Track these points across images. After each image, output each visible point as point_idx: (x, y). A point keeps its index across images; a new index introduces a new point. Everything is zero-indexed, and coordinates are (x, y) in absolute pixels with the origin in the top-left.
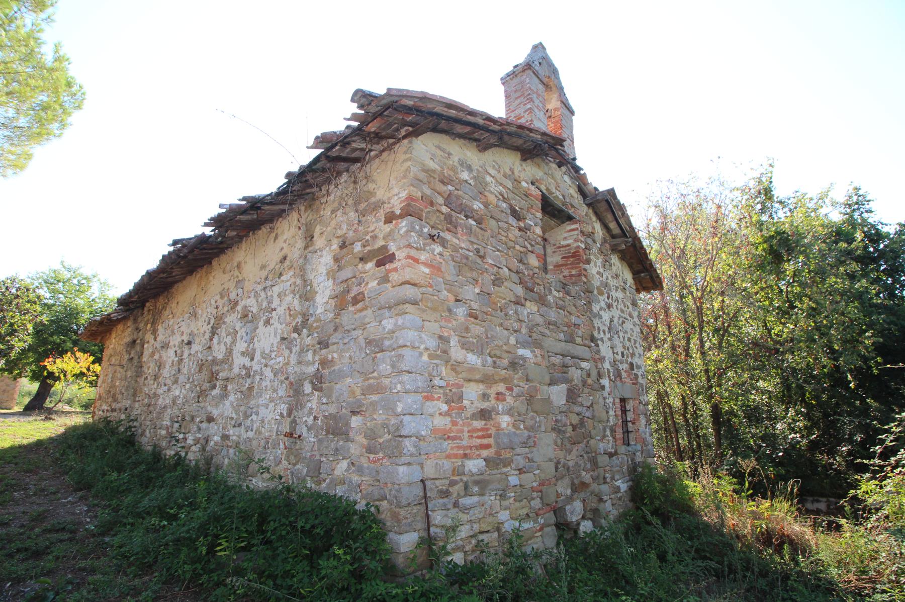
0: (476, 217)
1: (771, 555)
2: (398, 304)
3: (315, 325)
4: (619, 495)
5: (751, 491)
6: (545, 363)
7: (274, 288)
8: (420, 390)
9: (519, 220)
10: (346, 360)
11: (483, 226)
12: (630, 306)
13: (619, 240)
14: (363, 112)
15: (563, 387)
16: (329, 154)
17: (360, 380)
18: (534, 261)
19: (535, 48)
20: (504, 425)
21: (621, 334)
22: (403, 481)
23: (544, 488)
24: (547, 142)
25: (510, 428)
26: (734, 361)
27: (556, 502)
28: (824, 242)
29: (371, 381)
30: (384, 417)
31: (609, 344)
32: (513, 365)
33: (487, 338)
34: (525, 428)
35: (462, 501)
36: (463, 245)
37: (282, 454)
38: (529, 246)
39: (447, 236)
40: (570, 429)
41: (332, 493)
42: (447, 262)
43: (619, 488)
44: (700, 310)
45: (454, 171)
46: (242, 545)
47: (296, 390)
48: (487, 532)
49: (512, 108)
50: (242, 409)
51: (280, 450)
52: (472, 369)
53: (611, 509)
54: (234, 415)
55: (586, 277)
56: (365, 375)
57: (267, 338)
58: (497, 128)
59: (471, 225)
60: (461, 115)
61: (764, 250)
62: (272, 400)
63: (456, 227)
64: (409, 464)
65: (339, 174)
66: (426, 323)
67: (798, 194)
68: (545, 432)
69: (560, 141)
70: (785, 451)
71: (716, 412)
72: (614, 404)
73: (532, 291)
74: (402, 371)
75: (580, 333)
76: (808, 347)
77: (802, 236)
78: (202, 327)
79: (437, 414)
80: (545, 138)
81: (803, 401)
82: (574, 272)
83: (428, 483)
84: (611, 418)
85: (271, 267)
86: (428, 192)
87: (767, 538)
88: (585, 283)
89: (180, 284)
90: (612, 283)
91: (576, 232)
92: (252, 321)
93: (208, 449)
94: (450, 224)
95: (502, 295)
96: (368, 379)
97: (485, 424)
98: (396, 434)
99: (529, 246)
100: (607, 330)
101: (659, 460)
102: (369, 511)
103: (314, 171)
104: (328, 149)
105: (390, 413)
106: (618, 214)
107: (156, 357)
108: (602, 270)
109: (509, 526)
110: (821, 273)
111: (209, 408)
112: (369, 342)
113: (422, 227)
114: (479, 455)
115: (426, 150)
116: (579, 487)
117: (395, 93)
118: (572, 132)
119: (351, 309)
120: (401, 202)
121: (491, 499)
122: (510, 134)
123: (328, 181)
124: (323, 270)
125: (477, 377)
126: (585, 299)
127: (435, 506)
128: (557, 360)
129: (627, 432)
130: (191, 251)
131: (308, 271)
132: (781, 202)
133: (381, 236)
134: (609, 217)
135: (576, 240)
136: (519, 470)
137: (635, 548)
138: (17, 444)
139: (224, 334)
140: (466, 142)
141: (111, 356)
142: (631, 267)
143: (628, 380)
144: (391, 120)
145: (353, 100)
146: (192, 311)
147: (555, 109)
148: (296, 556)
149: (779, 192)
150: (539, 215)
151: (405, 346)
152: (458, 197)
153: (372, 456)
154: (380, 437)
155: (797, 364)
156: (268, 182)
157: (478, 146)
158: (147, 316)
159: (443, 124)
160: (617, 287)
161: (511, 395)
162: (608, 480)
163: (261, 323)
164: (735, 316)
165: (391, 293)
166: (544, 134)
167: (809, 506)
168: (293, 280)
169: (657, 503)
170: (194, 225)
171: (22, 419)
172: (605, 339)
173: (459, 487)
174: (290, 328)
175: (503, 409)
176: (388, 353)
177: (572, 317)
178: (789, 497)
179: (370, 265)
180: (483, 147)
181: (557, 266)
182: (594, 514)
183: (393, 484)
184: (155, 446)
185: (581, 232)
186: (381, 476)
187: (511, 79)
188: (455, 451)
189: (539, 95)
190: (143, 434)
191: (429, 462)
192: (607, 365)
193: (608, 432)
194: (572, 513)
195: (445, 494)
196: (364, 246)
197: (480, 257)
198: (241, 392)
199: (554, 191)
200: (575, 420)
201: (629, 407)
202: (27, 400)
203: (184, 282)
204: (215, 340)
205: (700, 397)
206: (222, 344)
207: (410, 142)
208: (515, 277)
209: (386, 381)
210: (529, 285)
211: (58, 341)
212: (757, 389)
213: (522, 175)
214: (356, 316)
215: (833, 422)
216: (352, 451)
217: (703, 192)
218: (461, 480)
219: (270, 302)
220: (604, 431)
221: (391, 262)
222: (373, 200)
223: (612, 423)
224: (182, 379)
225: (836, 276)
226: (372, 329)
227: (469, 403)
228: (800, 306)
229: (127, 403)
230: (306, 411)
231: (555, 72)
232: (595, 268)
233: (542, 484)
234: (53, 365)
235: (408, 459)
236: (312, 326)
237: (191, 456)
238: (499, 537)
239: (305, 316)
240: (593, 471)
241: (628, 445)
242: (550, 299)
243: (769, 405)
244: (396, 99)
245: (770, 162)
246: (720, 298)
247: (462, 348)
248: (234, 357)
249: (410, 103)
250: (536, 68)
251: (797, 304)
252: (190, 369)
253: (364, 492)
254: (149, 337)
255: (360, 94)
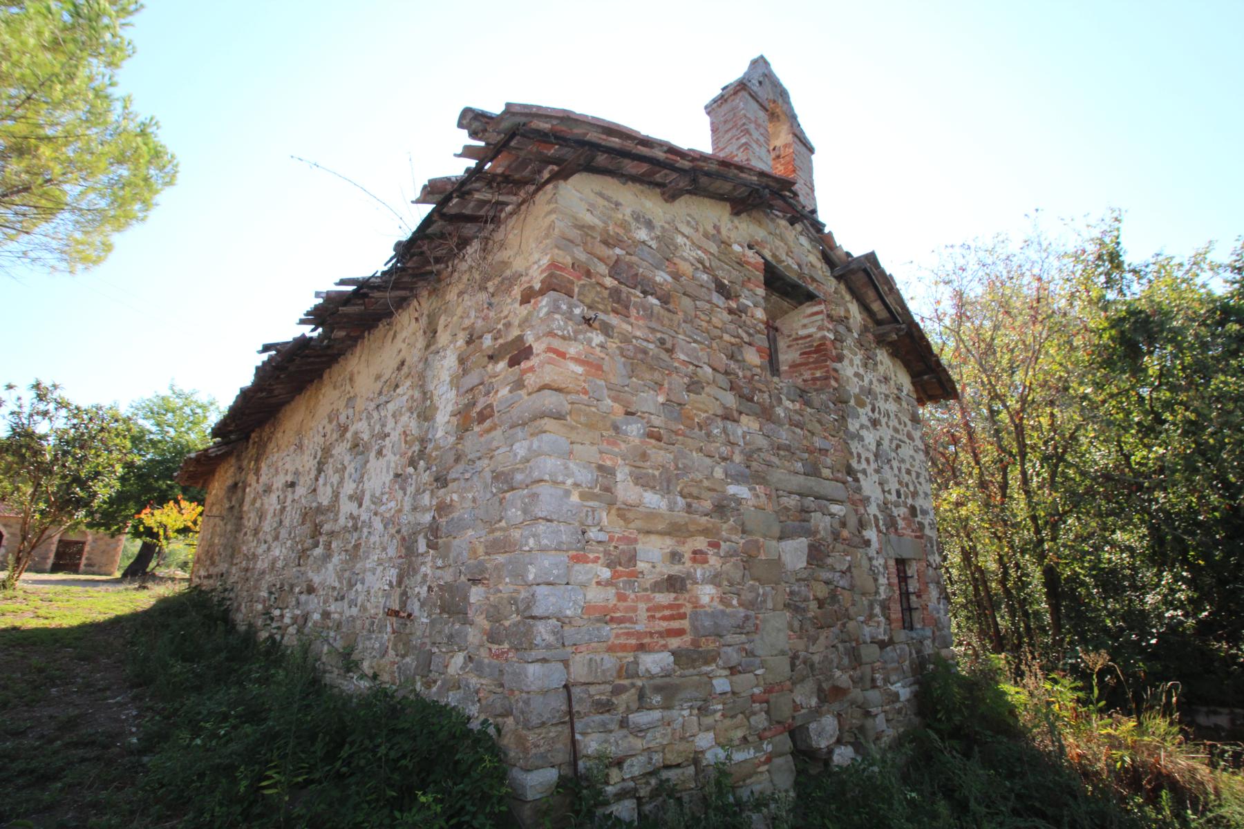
0: (659, 292)
1: (1139, 806)
2: (534, 419)
3: (434, 454)
4: (898, 705)
5: (1102, 703)
6: (770, 508)
7: (389, 405)
8: (565, 547)
9: (728, 298)
10: (469, 504)
11: (671, 306)
12: (909, 423)
13: (887, 328)
14: (482, 144)
15: (803, 542)
16: (445, 210)
17: (483, 532)
18: (752, 357)
19: (755, 63)
20: (705, 600)
21: (895, 464)
22: (533, 688)
23: (772, 697)
24: (767, 186)
25: (716, 603)
26: (1076, 501)
27: (793, 718)
28: (1203, 324)
29: (497, 534)
30: (511, 587)
31: (876, 477)
32: (721, 509)
33: (677, 468)
34: (741, 605)
35: (633, 718)
36: (638, 334)
37: (389, 640)
38: (744, 335)
39: (614, 320)
40: (813, 605)
41: (443, 702)
42: (612, 358)
43: (897, 695)
44: (1020, 430)
45: (624, 228)
46: (300, 779)
47: (408, 548)
48: (678, 766)
49: (721, 145)
50: (347, 574)
51: (387, 636)
52: (652, 515)
53: (884, 727)
54: (336, 584)
55: (836, 380)
56: (491, 525)
57: (379, 475)
58: (686, 164)
59: (652, 305)
60: (629, 145)
61: (1112, 338)
62: (380, 562)
63: (627, 307)
64: (544, 660)
65: (464, 243)
66: (577, 447)
67: (1160, 258)
68: (774, 610)
69: (787, 184)
70: (1160, 636)
71: (1051, 576)
72: (886, 567)
73: (751, 400)
74: (537, 519)
75: (829, 461)
76: (1187, 480)
77: (1168, 315)
78: (307, 462)
79: (594, 584)
80: (764, 180)
81: (1185, 561)
82: (818, 374)
83: (576, 691)
84: (882, 589)
85: (386, 377)
86: (582, 256)
87: (1133, 777)
88: (835, 389)
89: (288, 407)
90: (878, 390)
91: (820, 317)
92: (363, 453)
93: (306, 630)
94: (618, 302)
95: (702, 406)
96: (493, 531)
97: (676, 599)
98: (526, 614)
99: (744, 335)
100: (872, 458)
101: (963, 648)
102: (485, 732)
103: (430, 238)
104: (441, 204)
105: (521, 582)
106: (884, 289)
107: (258, 505)
108: (861, 371)
109: (714, 755)
110: (1203, 370)
111: (310, 574)
112: (497, 476)
113: (571, 307)
114: (665, 646)
115: (578, 198)
116: (830, 695)
117: (518, 109)
118: (811, 176)
119: (477, 429)
120: (542, 272)
121: (683, 714)
122: (708, 174)
123: (451, 255)
124: (445, 376)
125: (660, 527)
126: (836, 413)
127: (587, 725)
128: (792, 502)
129: (908, 610)
130: (291, 360)
131: (429, 379)
132: (1134, 272)
133: (516, 323)
134: (871, 294)
135: (820, 328)
136: (731, 668)
137: (920, 793)
138: (88, 621)
139: (330, 472)
140: (644, 188)
141: (213, 504)
142: (908, 366)
143: (908, 532)
144: (522, 154)
145: (460, 125)
146: (297, 442)
147: (786, 146)
148: (377, 800)
149: (1131, 257)
150: (761, 291)
151: (542, 481)
152: (630, 266)
153: (494, 647)
154: (506, 618)
155: (1173, 506)
156: (374, 260)
157: (663, 194)
158: (252, 451)
159: (601, 159)
160: (887, 396)
161: (717, 554)
162: (879, 683)
163: (373, 454)
164: (1073, 437)
165: (527, 402)
166: (762, 174)
167: (1202, 720)
168: (410, 392)
169: (957, 719)
170: (289, 327)
171: (121, 587)
172: (870, 470)
173: (628, 697)
174: (405, 461)
175: (703, 575)
176: (520, 492)
177: (815, 439)
178: (1167, 711)
179: (502, 365)
180: (671, 196)
181: (794, 366)
182: (855, 736)
183: (522, 691)
184: (250, 625)
185: (828, 316)
186: (506, 679)
187: (719, 106)
188: (622, 641)
189: (758, 126)
190: (238, 609)
191: (578, 657)
192: (873, 509)
193: (877, 610)
194: (819, 735)
195: (605, 707)
196: (496, 339)
197: (667, 350)
198: (346, 551)
199: (784, 257)
200: (822, 591)
201: (911, 570)
202: (127, 563)
203: (293, 404)
204: (321, 481)
205: (1027, 556)
206: (328, 486)
207: (556, 187)
208: (721, 379)
209: (516, 534)
210: (746, 391)
211: (164, 487)
212: (1113, 545)
213: (733, 235)
214: (483, 439)
215: (1233, 592)
216: (470, 638)
217: (1014, 259)
218: (633, 685)
219: (383, 426)
220: (871, 607)
221: (527, 358)
222: (508, 273)
223: (883, 596)
224: (283, 533)
225: (1224, 373)
226: (500, 458)
227: (648, 566)
228: (1170, 418)
229: (223, 567)
230: (419, 578)
231: (784, 94)
232: (851, 368)
233: (769, 690)
234: (153, 518)
235: (541, 653)
236: (430, 456)
237: (286, 641)
238: (697, 774)
239: (423, 441)
240: (854, 669)
241: (912, 628)
242: (780, 411)
243: (1134, 568)
244: (523, 120)
245: (1115, 215)
246: (1048, 410)
247: (636, 484)
248: (341, 502)
249: (545, 126)
250: (755, 88)
251: (1167, 416)
252: (292, 521)
253: (484, 702)
254: (252, 478)
255: (470, 115)
